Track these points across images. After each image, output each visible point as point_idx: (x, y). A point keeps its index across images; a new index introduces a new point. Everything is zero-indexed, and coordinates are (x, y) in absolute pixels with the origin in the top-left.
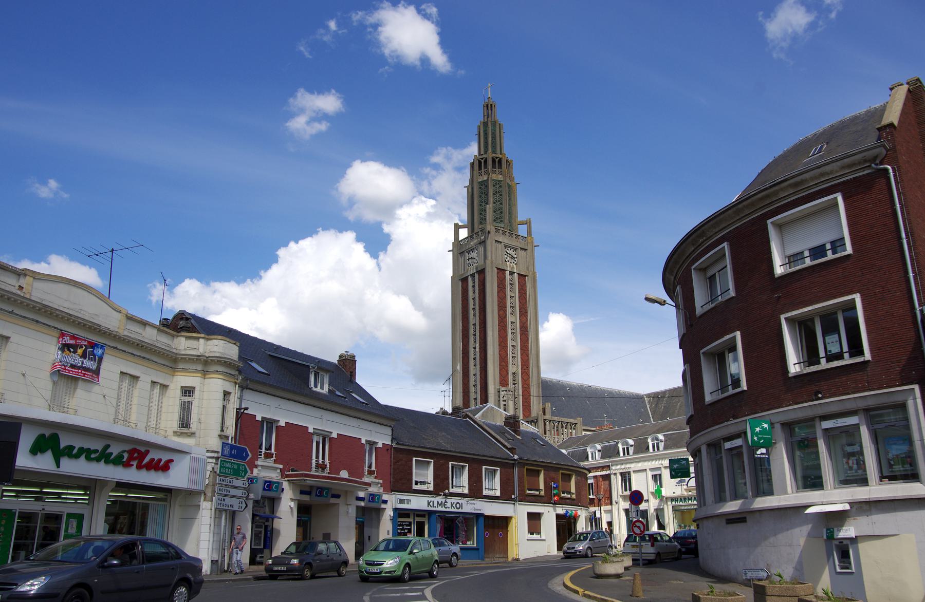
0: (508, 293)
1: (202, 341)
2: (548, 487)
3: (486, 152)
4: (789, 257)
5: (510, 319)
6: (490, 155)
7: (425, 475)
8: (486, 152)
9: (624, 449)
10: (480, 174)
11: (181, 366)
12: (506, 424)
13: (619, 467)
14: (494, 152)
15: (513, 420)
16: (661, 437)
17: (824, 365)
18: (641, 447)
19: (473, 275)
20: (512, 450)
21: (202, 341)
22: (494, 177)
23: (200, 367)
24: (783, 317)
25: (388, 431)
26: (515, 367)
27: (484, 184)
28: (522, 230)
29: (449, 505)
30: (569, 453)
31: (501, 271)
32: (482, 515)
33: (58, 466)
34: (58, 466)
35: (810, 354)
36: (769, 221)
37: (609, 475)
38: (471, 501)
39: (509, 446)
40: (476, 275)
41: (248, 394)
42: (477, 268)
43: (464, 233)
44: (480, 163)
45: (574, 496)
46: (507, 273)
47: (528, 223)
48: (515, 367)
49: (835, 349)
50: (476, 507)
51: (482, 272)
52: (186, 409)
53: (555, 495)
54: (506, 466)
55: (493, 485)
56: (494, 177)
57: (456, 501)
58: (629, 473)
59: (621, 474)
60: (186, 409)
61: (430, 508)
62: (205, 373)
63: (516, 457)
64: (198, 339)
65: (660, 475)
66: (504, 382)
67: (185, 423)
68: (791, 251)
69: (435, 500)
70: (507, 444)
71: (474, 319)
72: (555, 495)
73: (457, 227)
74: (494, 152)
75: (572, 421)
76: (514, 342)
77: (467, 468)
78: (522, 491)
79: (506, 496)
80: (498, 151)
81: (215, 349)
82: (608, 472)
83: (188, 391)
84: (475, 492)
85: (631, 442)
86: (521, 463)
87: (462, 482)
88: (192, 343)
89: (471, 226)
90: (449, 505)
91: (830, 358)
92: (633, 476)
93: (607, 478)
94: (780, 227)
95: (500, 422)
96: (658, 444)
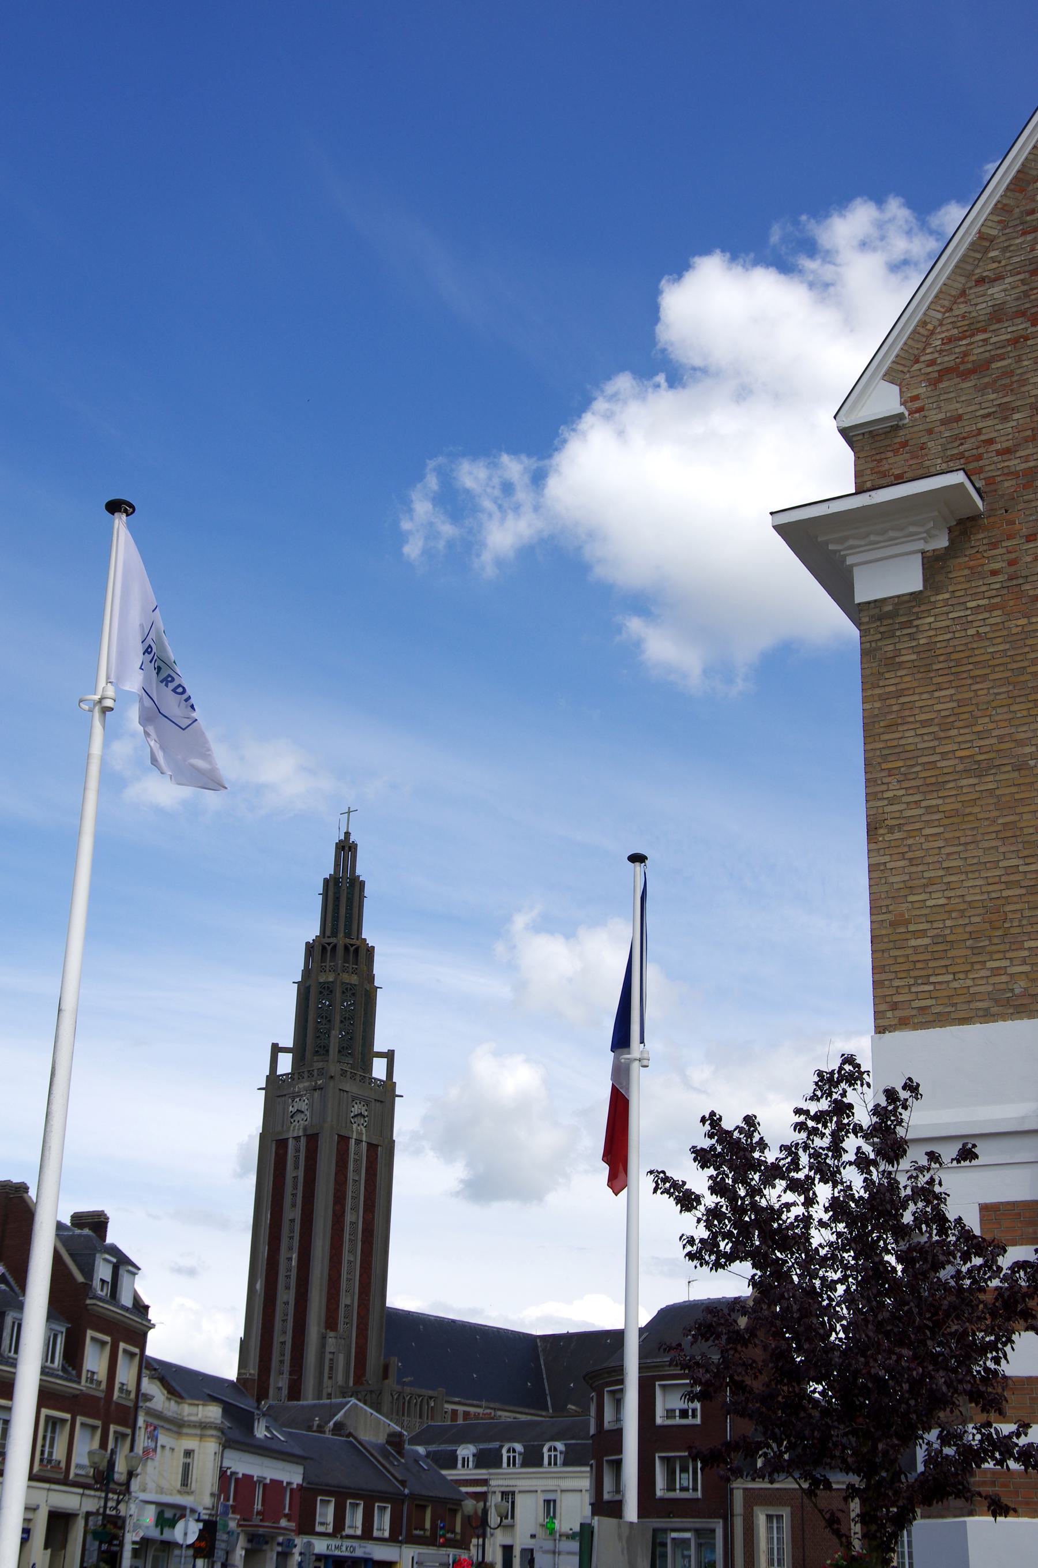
0: (351, 1175)
1: (200, 1407)
2: (434, 1526)
3: (334, 934)
4: (667, 1411)
5: (349, 1217)
6: (341, 940)
7: (326, 1514)
8: (334, 934)
9: (509, 1458)
10: (323, 970)
11: (185, 1430)
12: (388, 1442)
13: (500, 1482)
14: (348, 935)
15: (398, 1440)
16: (560, 1446)
17: (678, 1494)
18: (532, 1459)
19: (297, 1139)
20: (403, 1483)
21: (200, 1407)
22: (345, 977)
23: (198, 1432)
24: (657, 1455)
25: (300, 1469)
26: (348, 1299)
27: (326, 989)
28: (379, 1069)
29: (344, 1548)
30: (428, 1455)
31: (344, 1140)
32: (371, 1560)
33: (162, 1533)
34: (162, 1533)
35: (671, 1487)
36: (657, 1383)
37: (485, 1494)
38: (363, 1543)
39: (400, 1478)
40: (303, 1140)
41: (228, 1453)
42: (305, 1129)
43: (285, 1064)
44: (324, 948)
45: (458, 1537)
46: (353, 1142)
47: (390, 1056)
48: (348, 1299)
49: (685, 1484)
50: (367, 1550)
51: (312, 1139)
52: (186, 1469)
53: (441, 1536)
54: (396, 1500)
55: (383, 1524)
56: (345, 977)
57: (350, 1544)
58: (513, 1493)
59: (503, 1493)
60: (186, 1469)
61: (329, 1553)
62: (202, 1437)
63: (407, 1491)
64: (198, 1405)
65: (555, 1501)
66: (331, 1323)
67: (185, 1481)
68: (669, 1406)
69: (334, 1542)
70: (397, 1475)
71: (292, 1213)
72: (441, 1536)
73: (276, 1049)
74: (348, 935)
75: (431, 1393)
76: (351, 1256)
77: (361, 1507)
78: (409, 1531)
79: (394, 1539)
80: (354, 935)
81: (210, 1414)
82: (483, 1489)
83: (188, 1453)
84: (367, 1534)
85: (519, 1447)
86: (412, 1496)
87: (355, 1520)
88: (193, 1409)
89: (299, 1051)
90: (344, 1548)
91: (682, 1489)
92: (519, 1499)
93: (482, 1497)
94: (663, 1387)
95: (382, 1439)
96: (555, 1456)
